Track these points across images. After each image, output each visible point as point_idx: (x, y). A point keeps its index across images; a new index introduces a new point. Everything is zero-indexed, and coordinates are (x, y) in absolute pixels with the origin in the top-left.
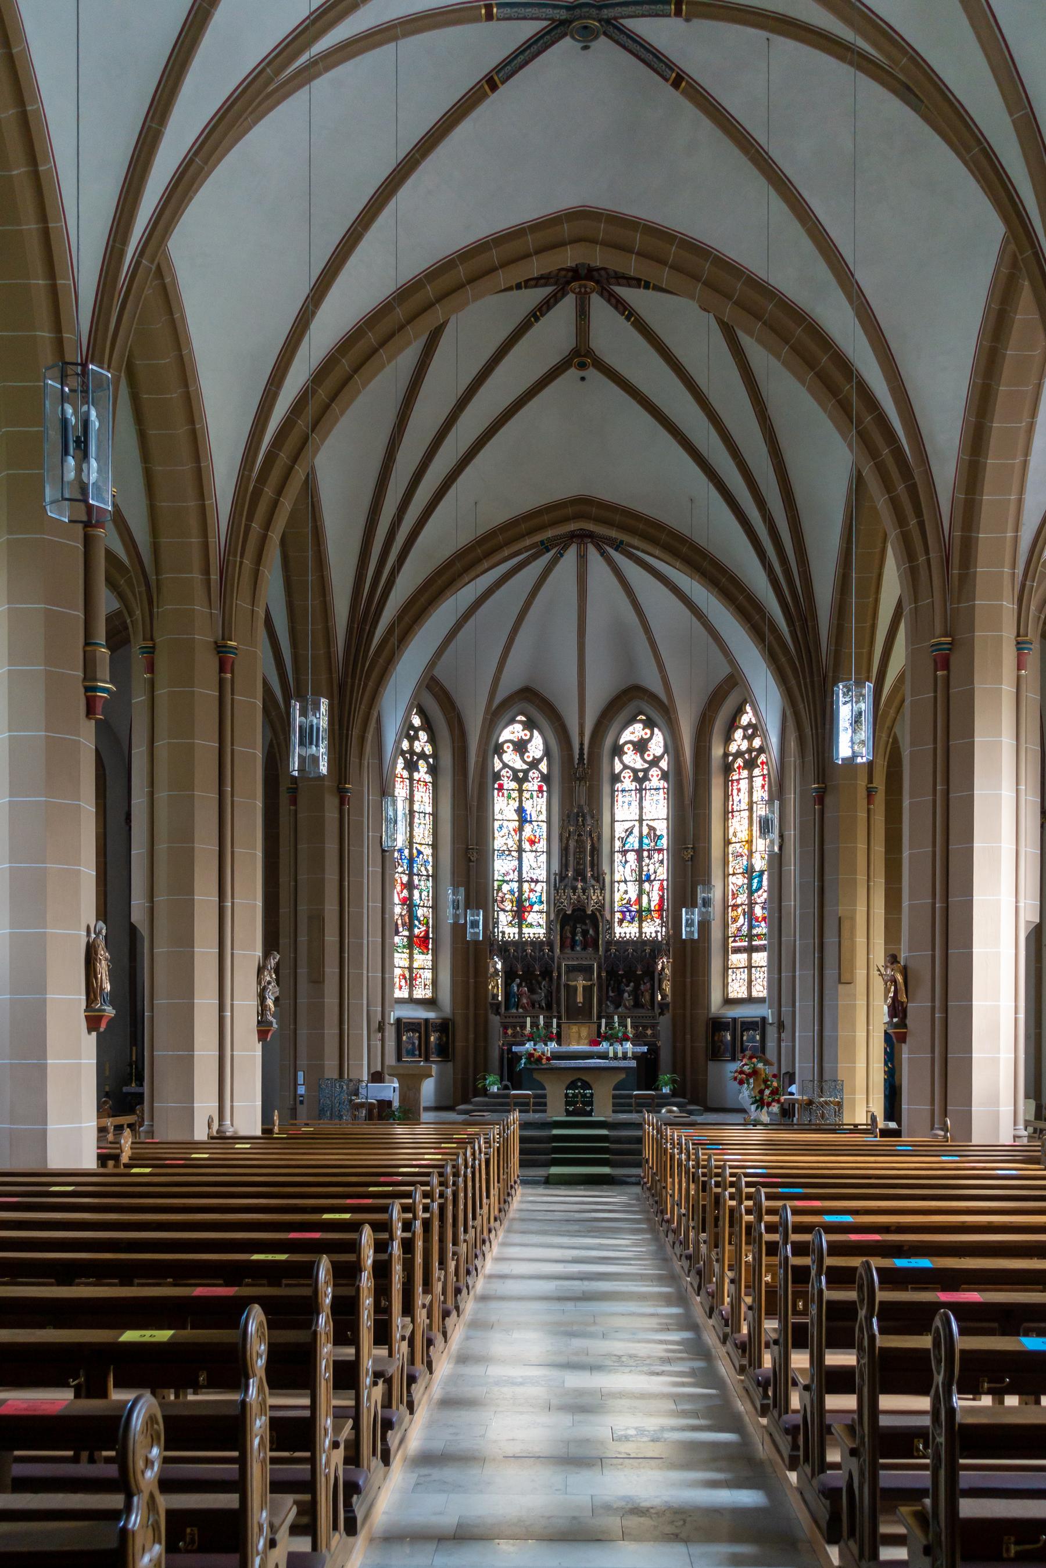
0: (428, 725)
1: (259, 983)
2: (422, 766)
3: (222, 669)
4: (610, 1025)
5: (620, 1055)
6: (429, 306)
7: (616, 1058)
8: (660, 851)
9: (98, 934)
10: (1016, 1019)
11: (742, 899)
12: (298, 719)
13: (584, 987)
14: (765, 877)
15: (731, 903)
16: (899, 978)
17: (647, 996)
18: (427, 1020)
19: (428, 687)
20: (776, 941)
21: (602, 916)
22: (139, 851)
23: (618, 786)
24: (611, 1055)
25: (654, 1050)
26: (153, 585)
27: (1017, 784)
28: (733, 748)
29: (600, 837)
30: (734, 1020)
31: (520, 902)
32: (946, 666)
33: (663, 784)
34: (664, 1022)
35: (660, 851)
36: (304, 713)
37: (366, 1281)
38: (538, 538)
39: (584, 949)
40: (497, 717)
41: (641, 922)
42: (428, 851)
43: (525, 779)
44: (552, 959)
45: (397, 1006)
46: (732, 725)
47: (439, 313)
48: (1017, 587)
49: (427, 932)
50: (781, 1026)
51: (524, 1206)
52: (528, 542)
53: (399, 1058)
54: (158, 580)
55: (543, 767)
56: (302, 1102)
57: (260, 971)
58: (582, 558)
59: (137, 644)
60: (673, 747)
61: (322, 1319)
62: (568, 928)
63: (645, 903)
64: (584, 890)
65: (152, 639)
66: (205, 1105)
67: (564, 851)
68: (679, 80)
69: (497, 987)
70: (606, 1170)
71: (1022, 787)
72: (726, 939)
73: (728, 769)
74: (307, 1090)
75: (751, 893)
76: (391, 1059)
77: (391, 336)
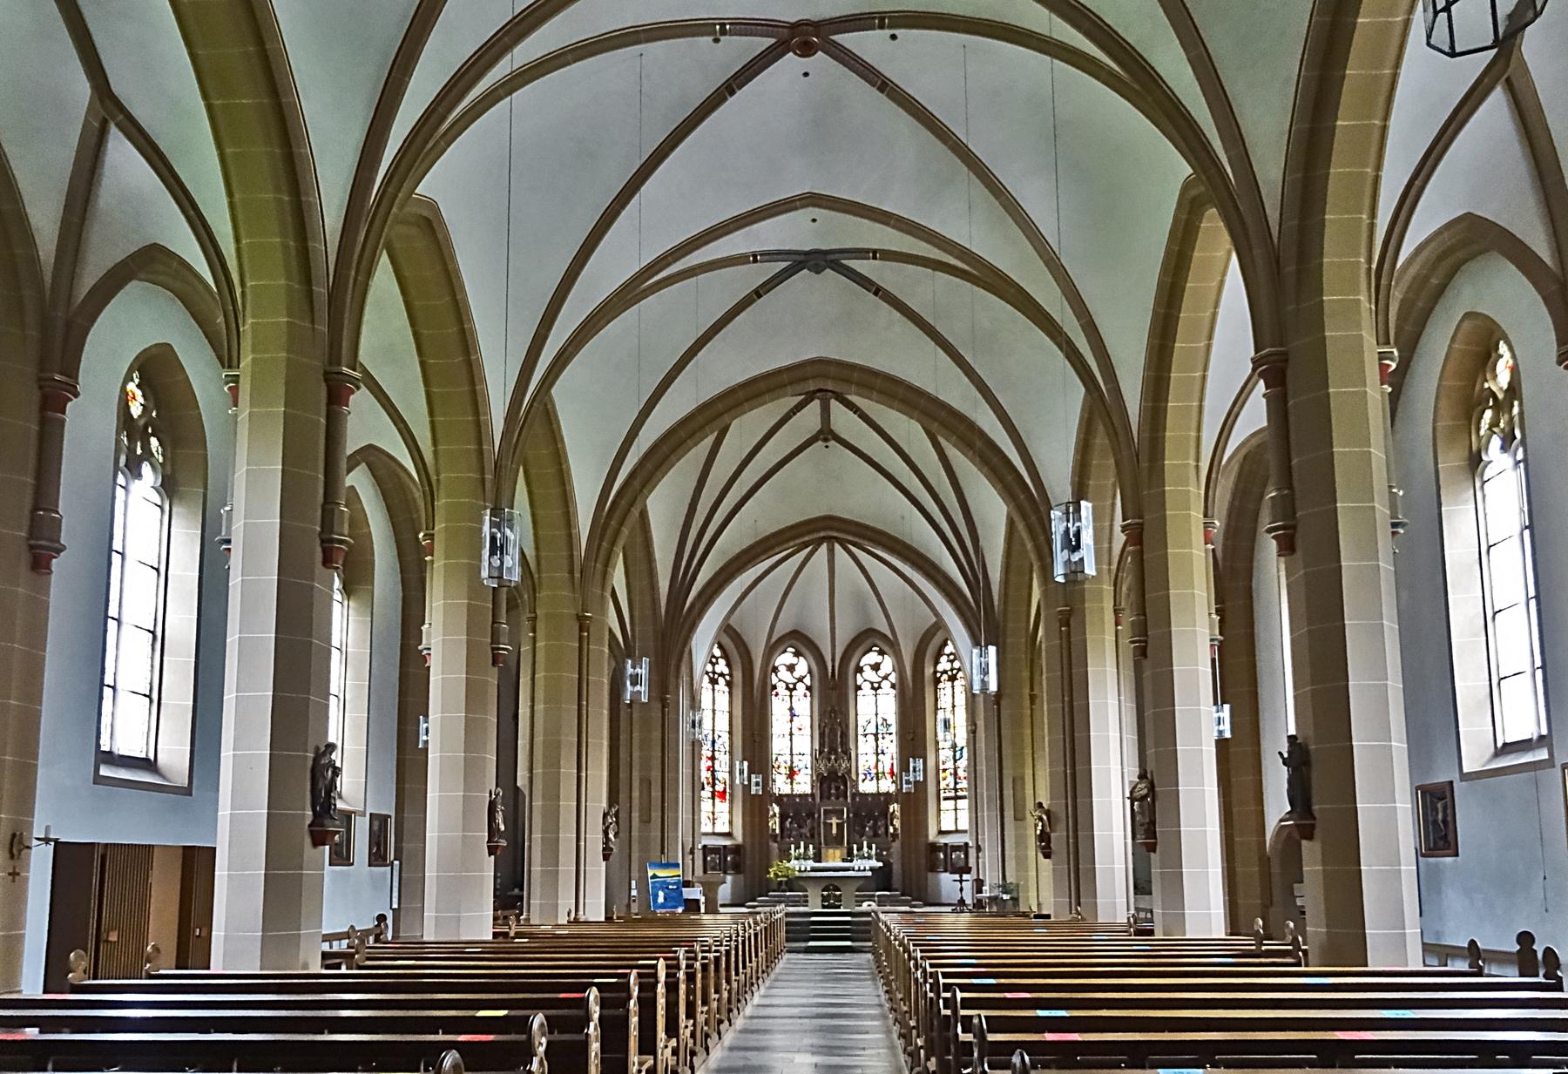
0: (725, 656)
1: (604, 824)
2: (721, 680)
3: (581, 630)
4: (860, 848)
5: (803, 869)
6: (721, 414)
7: (859, 870)
8: (890, 734)
9: (497, 795)
10: (1125, 843)
11: (950, 765)
12: (630, 671)
13: (838, 824)
14: (965, 750)
15: (942, 767)
16: (1045, 817)
17: (883, 829)
18: (725, 847)
19: (725, 631)
20: (973, 793)
21: (850, 777)
22: (523, 743)
23: (859, 692)
24: (856, 868)
25: (888, 865)
26: (536, 581)
27: (1119, 696)
28: (940, 668)
29: (847, 726)
30: (946, 844)
31: (791, 768)
32: (1068, 625)
33: (893, 692)
34: (896, 845)
35: (890, 734)
36: (634, 667)
37: (661, 989)
38: (802, 540)
39: (837, 798)
40: (773, 649)
41: (878, 779)
42: (726, 737)
43: (795, 689)
44: (814, 805)
45: (703, 837)
46: (939, 653)
47: (726, 417)
48: (1113, 578)
49: (725, 789)
50: (979, 849)
51: (788, 966)
52: (791, 544)
53: (705, 872)
54: (539, 577)
55: (807, 681)
56: (634, 901)
57: (605, 815)
58: (831, 551)
59: (525, 615)
60: (899, 667)
61: (632, 1002)
62: (825, 785)
63: (880, 770)
64: (836, 760)
65: (535, 612)
66: (566, 902)
67: (822, 735)
68: (878, 291)
69: (775, 824)
70: (848, 943)
71: (1122, 698)
72: (939, 791)
73: (937, 681)
74: (638, 893)
75: (955, 761)
76: (699, 871)
77: (694, 433)
